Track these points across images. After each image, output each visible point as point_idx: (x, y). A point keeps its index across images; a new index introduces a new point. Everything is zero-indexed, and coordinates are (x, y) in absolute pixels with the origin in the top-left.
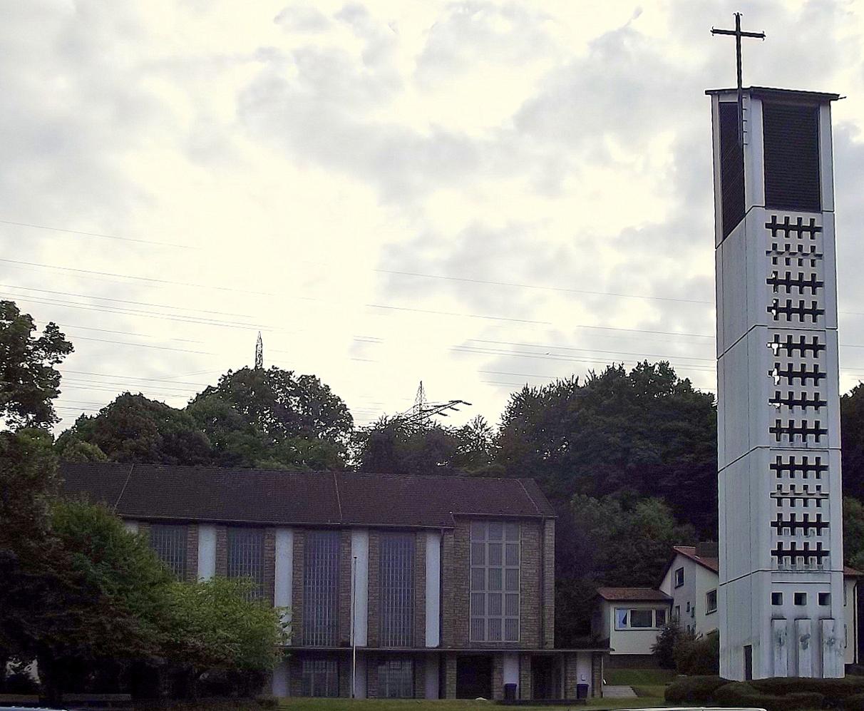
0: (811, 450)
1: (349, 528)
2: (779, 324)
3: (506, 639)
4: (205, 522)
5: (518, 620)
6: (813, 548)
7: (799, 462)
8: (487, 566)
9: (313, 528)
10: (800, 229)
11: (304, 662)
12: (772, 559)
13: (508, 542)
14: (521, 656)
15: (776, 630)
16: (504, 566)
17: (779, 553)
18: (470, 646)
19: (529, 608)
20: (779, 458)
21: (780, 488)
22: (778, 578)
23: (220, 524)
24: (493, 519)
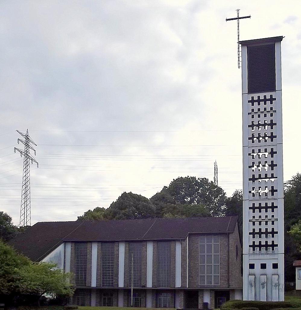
0: (269, 199)
1: (146, 241)
6: (270, 243)
8: (206, 254)
11: (163, 294)
12: (249, 249)
14: (211, 290)
17: (254, 246)
18: (199, 287)
20: (254, 204)
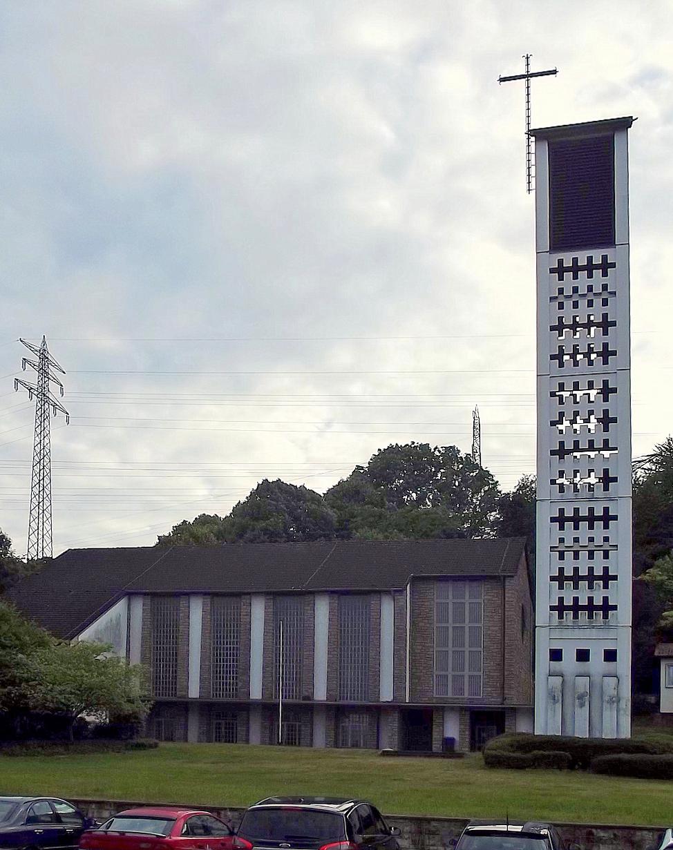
3: (469, 695)
4: (193, 593)
5: (480, 676)
6: (598, 602)
7: (584, 512)
9: (347, 593)
10: (590, 268)
13: (455, 601)
21: (562, 540)
23: (205, 594)
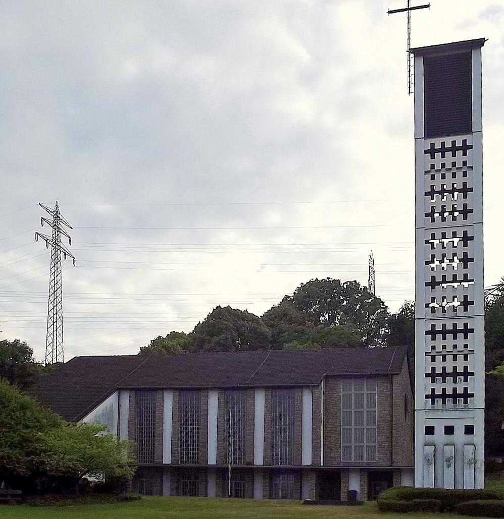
0: (459, 318)
1: (253, 388)
2: (436, 225)
14: (362, 471)
15: (425, 453)
16: (365, 409)
19: (383, 438)
22: (430, 415)
24: (356, 377)
